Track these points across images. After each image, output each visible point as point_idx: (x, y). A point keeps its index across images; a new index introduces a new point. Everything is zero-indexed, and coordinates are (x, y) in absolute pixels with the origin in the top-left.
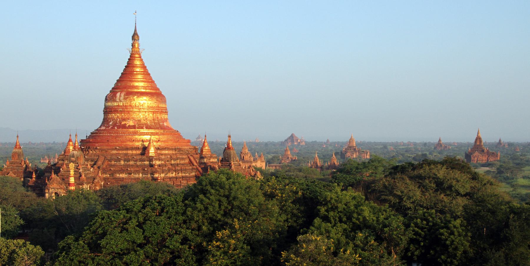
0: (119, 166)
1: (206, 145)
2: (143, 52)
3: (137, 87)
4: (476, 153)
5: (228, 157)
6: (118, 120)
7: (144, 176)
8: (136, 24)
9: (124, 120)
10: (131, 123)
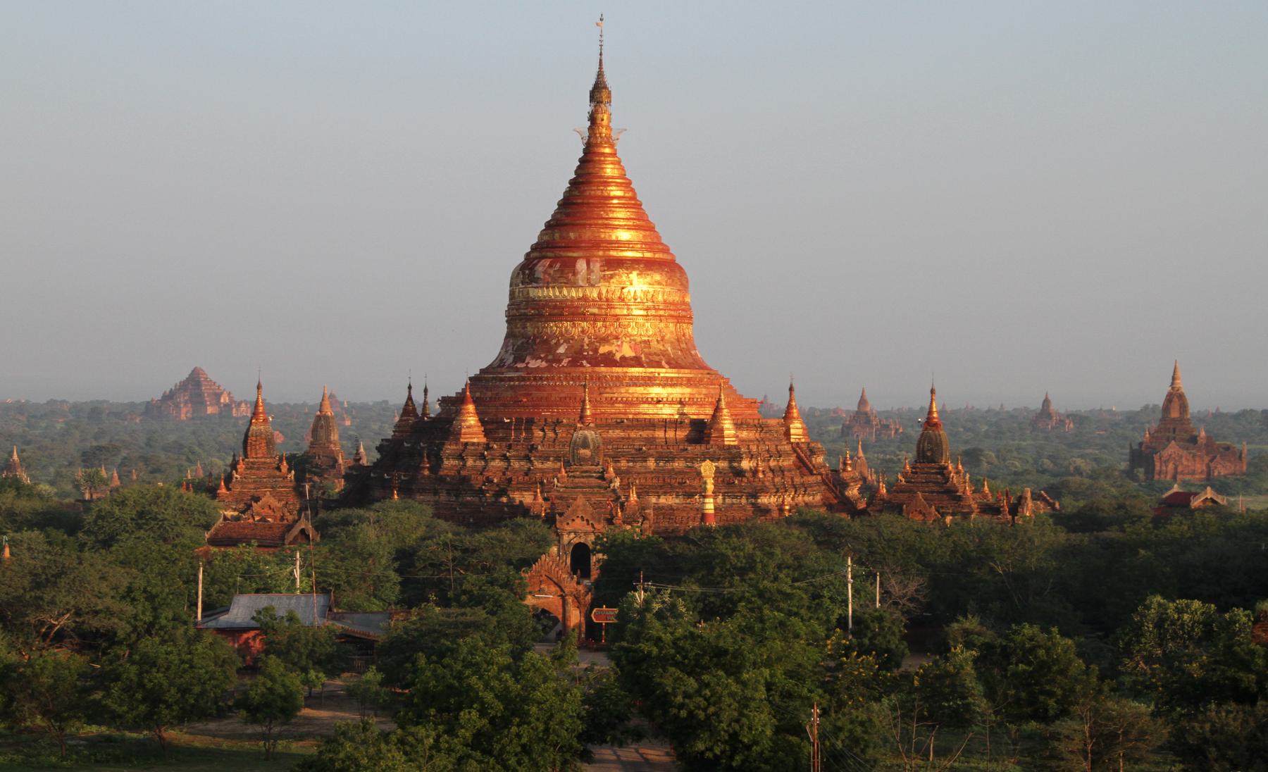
0: (645, 473)
1: (795, 415)
2: (621, 137)
3: (619, 244)
4: (1173, 449)
5: (931, 450)
6: (586, 340)
7: (728, 501)
8: (601, 54)
9: (605, 340)
10: (627, 352)
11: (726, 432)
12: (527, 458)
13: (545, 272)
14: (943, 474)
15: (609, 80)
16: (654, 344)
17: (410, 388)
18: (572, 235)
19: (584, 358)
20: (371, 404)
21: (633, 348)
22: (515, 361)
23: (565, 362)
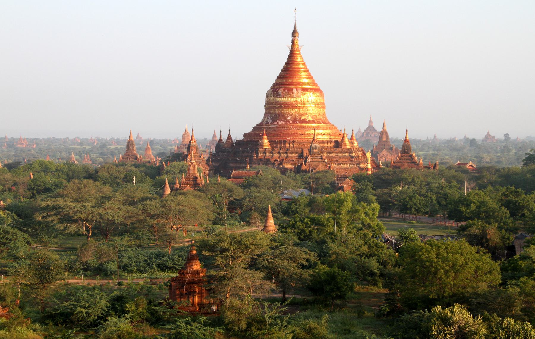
3: (303, 84)
4: (384, 152)
5: (407, 149)
6: (297, 115)
7: (351, 166)
9: (303, 115)
11: (347, 144)
12: (286, 153)
13: (282, 93)
14: (411, 157)
15: (298, 29)
16: (318, 116)
17: (229, 130)
18: (290, 81)
19: (297, 121)
20: (41, 138)
21: (312, 117)
22: (273, 121)
23: (291, 122)
